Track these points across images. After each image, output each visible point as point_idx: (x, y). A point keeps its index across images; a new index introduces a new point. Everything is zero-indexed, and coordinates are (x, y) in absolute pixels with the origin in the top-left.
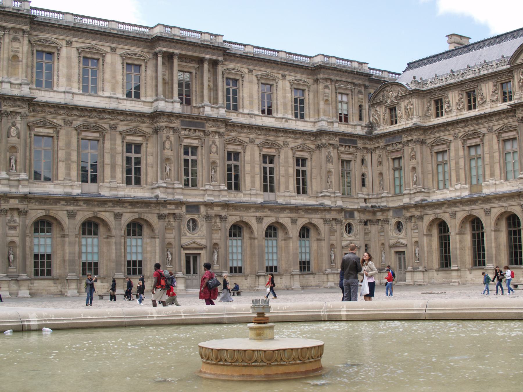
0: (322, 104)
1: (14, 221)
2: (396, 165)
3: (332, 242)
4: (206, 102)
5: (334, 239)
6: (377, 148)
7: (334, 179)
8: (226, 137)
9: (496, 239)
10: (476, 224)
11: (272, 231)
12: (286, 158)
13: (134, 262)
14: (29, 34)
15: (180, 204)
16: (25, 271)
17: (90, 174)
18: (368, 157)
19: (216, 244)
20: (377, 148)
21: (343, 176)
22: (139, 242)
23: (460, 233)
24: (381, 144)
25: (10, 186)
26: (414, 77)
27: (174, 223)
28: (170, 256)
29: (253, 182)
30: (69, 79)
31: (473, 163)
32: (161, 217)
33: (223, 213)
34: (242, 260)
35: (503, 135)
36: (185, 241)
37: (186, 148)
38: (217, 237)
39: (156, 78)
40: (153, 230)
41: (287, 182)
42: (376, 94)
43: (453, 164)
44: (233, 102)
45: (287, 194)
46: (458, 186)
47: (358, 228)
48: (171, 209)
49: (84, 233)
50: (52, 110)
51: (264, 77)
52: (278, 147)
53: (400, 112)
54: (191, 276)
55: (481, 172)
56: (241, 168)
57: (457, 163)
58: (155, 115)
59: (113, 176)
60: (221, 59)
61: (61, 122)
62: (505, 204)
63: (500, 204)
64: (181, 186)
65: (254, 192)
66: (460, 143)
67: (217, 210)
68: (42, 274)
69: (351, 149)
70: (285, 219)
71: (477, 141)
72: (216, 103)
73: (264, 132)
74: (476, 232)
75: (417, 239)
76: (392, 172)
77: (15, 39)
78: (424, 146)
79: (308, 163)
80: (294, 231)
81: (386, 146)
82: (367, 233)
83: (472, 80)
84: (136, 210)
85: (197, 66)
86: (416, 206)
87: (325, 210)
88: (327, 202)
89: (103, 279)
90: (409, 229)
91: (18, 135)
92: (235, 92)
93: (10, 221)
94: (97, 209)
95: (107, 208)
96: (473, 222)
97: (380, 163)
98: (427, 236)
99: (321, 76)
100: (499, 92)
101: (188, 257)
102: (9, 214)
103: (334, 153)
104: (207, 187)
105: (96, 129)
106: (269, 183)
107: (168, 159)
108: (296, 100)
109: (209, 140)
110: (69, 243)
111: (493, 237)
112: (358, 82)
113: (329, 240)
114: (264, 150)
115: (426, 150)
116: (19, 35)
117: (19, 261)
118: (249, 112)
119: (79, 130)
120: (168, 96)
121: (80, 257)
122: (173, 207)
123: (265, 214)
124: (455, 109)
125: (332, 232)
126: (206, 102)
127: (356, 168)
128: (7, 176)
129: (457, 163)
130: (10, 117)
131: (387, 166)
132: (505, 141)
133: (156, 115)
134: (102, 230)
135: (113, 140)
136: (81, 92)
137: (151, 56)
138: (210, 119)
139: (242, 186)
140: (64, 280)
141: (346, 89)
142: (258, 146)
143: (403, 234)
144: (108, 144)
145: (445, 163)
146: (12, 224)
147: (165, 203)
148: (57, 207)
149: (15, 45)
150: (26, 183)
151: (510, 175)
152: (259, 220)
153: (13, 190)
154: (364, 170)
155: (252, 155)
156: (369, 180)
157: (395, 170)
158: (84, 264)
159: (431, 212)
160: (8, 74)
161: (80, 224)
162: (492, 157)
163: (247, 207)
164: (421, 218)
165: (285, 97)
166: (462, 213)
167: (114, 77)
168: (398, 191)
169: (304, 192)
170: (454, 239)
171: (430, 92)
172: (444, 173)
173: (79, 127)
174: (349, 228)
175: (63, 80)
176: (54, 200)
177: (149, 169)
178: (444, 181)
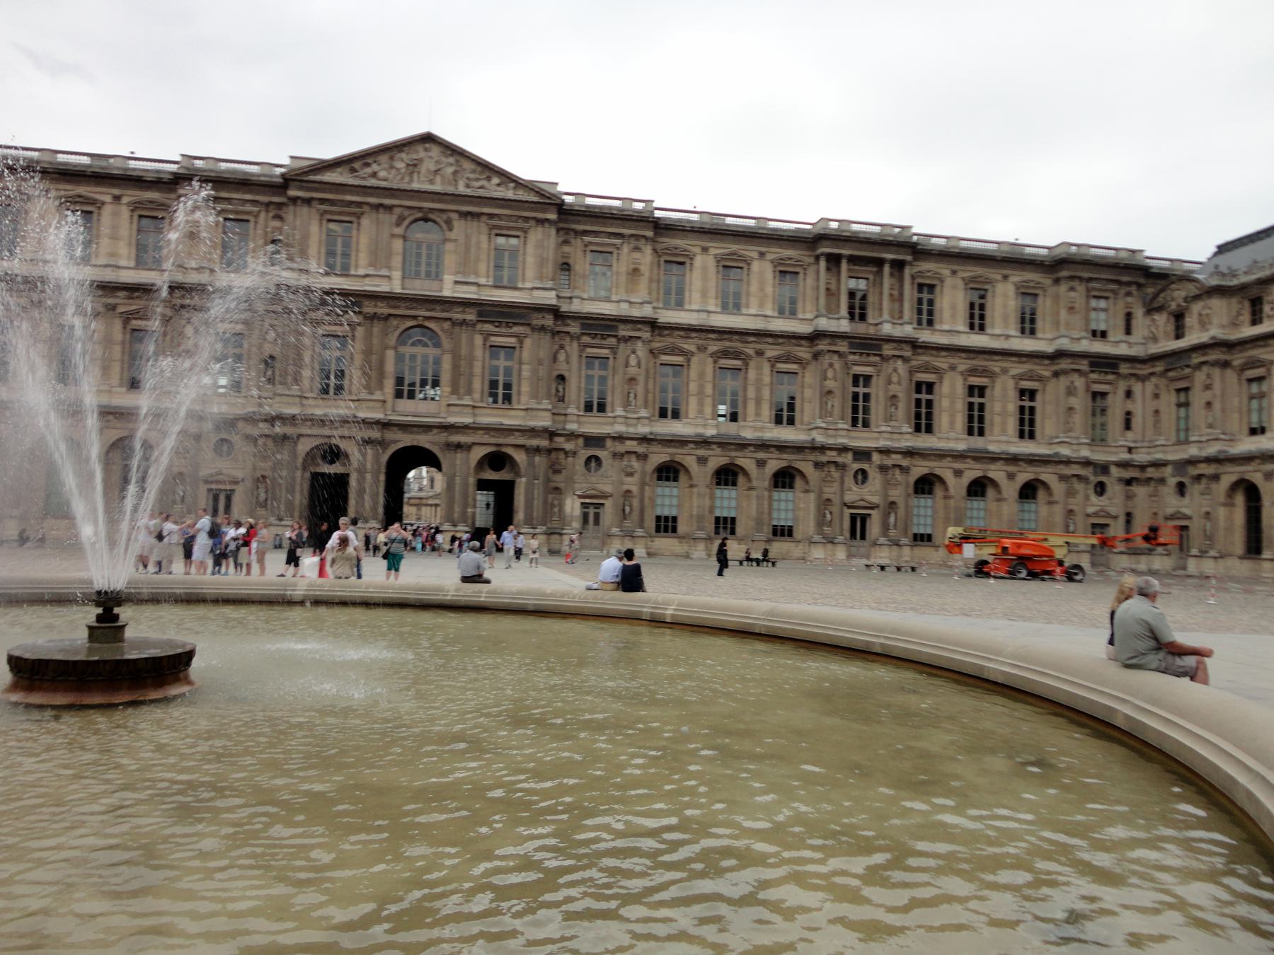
0: (1063, 314)
1: (631, 467)
2: (1182, 399)
3: (1071, 507)
4: (886, 316)
5: (1075, 503)
6: (1152, 374)
7: (1078, 419)
8: (914, 363)
11: (978, 488)
12: (1004, 389)
13: (725, 519)
14: (653, 240)
15: (844, 449)
16: (641, 527)
17: (786, 414)
18: (1137, 388)
19: (893, 503)
20: (1152, 374)
21: (1094, 415)
22: (929, 502)
24: (1159, 368)
25: (628, 425)
27: (836, 474)
28: (828, 516)
29: (952, 423)
30: (704, 294)
32: (818, 465)
33: (641, 449)
34: (933, 526)
36: (849, 498)
37: (856, 379)
38: (896, 494)
39: (818, 287)
40: (807, 482)
41: (1004, 424)
42: (1156, 296)
44: (926, 316)
45: (1003, 438)
47: (1115, 489)
48: (831, 456)
49: (776, 486)
50: (682, 333)
51: (973, 279)
52: (991, 375)
53: (1191, 320)
54: (858, 542)
56: (936, 404)
58: (815, 336)
59: (758, 414)
60: (909, 258)
61: (693, 348)
64: (846, 427)
65: (952, 435)
67: (897, 459)
68: (666, 531)
69: (1110, 377)
70: (997, 473)
72: (901, 317)
73: (972, 355)
75: (1208, 509)
76: (1174, 409)
77: (637, 249)
79: (1039, 397)
80: (1010, 490)
81: (1167, 370)
82: (1129, 497)
84: (785, 456)
85: (875, 269)
86: (1209, 460)
87: (1061, 462)
88: (1065, 451)
89: (741, 540)
90: (1196, 494)
91: (639, 365)
92: (931, 302)
93: (627, 466)
94: (734, 454)
95: (747, 452)
97: (1156, 396)
98: (1225, 505)
99: (1064, 273)
101: (853, 518)
102: (625, 458)
103: (1079, 382)
104: (883, 429)
105: (737, 355)
106: (976, 422)
107: (830, 392)
108: (972, 306)
109: (888, 368)
110: (699, 494)
112: (1125, 279)
113: (1066, 504)
114: (971, 379)
116: (641, 243)
117: (636, 515)
118: (951, 326)
119: (717, 356)
120: (831, 310)
121: (711, 511)
122: (834, 453)
123: (966, 466)
125: (1070, 493)
126: (886, 316)
127: (1116, 405)
128: (623, 413)
130: (557, 338)
131: (1169, 400)
133: (816, 336)
134: (741, 480)
135: (759, 368)
136: (719, 310)
137: (812, 260)
138: (890, 340)
139: (935, 427)
140: (690, 538)
141: (1106, 290)
142: (962, 374)
143: (1186, 500)
144: (752, 374)
145: (1261, 396)
146: (629, 470)
147: (823, 449)
148: (684, 451)
149: (637, 255)
150: (646, 422)
152: (958, 473)
153: (631, 430)
154: (1130, 406)
155: (953, 386)
156: (1137, 421)
157: (1179, 405)
158: (717, 519)
159: (1231, 469)
160: (627, 292)
161: (712, 471)
163: (941, 455)
164: (1216, 478)
165: (1005, 306)
167: (762, 290)
168: (1182, 435)
169: (1032, 436)
171: (1243, 288)
172: (1260, 410)
174: (1101, 489)
175: (696, 296)
176: (681, 442)
177: (807, 406)
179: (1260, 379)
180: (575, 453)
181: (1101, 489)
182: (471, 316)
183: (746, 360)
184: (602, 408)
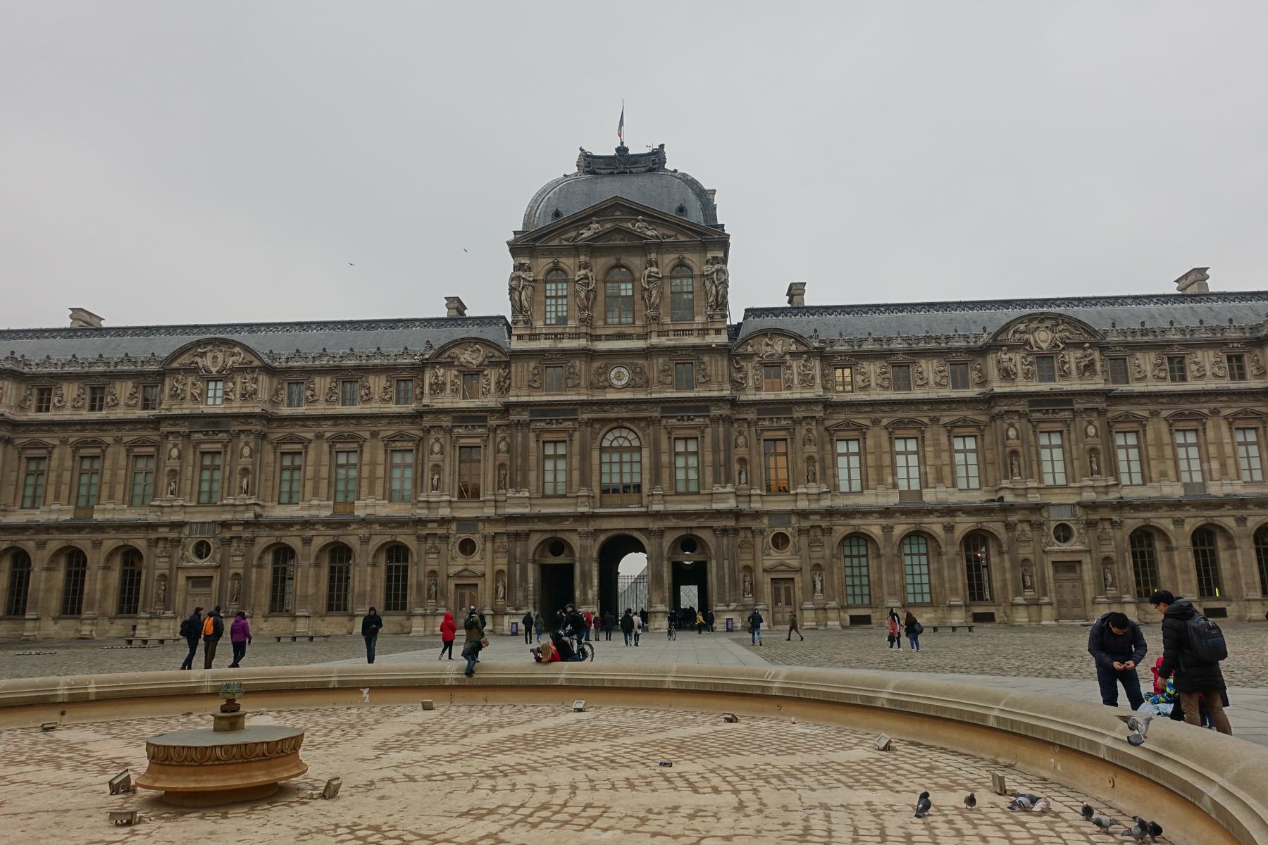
8: (1109, 415)
9: (104, 579)
10: (76, 559)
23: (107, 568)
26: (13, 353)
31: (85, 479)
32: (423, 539)
33: (247, 534)
35: (136, 450)
43: (52, 476)
46: (315, 502)
55: (94, 491)
57: (59, 476)
62: (124, 536)
63: (118, 536)
66: (69, 450)
71: (97, 451)
73: (1175, 400)
74: (394, 564)
78: (10, 447)
83: (103, 375)
86: (246, 524)
96: (70, 556)
100: (88, 397)
111: (99, 577)
115: (12, 453)
124: (69, 405)
129: (59, 476)
132: (137, 457)
143: (477, 557)
151: (137, 501)
162: (114, 475)
166: (110, 542)
170: (38, 578)
171: (35, 377)
172: (36, 486)
173: (893, 423)
178: (34, 497)
179: (40, 459)
180: (447, 537)
181: (467, 547)
182: (525, 417)
183: (306, 443)
184: (476, 494)
